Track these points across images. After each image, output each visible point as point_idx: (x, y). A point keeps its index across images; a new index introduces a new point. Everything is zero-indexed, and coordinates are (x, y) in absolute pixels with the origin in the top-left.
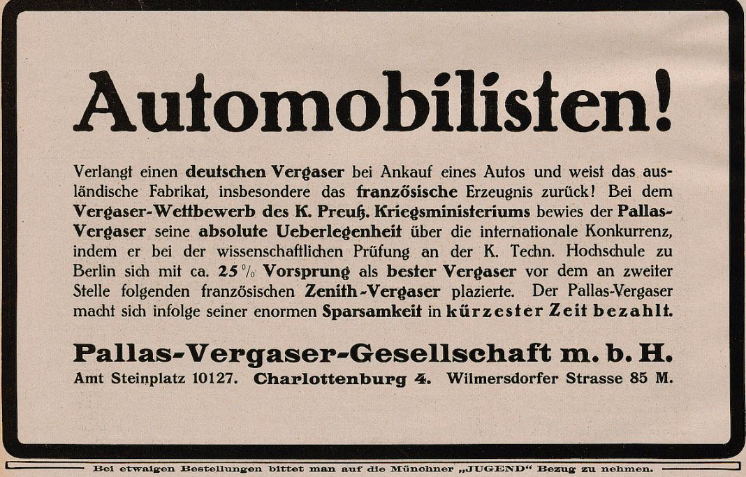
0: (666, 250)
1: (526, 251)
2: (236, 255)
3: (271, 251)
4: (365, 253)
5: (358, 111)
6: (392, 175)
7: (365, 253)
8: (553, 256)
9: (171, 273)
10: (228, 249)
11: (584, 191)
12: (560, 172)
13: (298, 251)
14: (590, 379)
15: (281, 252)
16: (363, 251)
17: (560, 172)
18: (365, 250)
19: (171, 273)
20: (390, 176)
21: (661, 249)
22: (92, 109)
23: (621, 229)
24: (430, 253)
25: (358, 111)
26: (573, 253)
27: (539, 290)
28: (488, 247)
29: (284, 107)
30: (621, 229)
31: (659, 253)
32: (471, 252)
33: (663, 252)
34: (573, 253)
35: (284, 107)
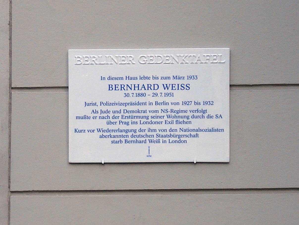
0: (164, 77)
1: (105, 130)
2: (183, 88)
3: (188, 136)
4: (123, 123)
5: (136, 112)
6: (95, 113)
7: (123, 123)
8: (130, 97)
9: (81, 118)
10: (118, 103)
11: (139, 111)
12: (121, 112)
13: (197, 136)
14: (143, 111)
15: (191, 136)
16: (122, 123)
17: (121, 112)
18: (123, 122)
19: (81, 118)
20: (94, 113)
21: (162, 77)
22: (92, 112)
23: (140, 111)
24: (164, 131)
25: (136, 112)
26: (127, 79)
27: (125, 111)
28: (76, 130)
29: (156, 111)
30: (140, 111)
31: (162, 78)
32: (145, 130)
33: (163, 78)
34: (127, 79)
35: (156, 111)
